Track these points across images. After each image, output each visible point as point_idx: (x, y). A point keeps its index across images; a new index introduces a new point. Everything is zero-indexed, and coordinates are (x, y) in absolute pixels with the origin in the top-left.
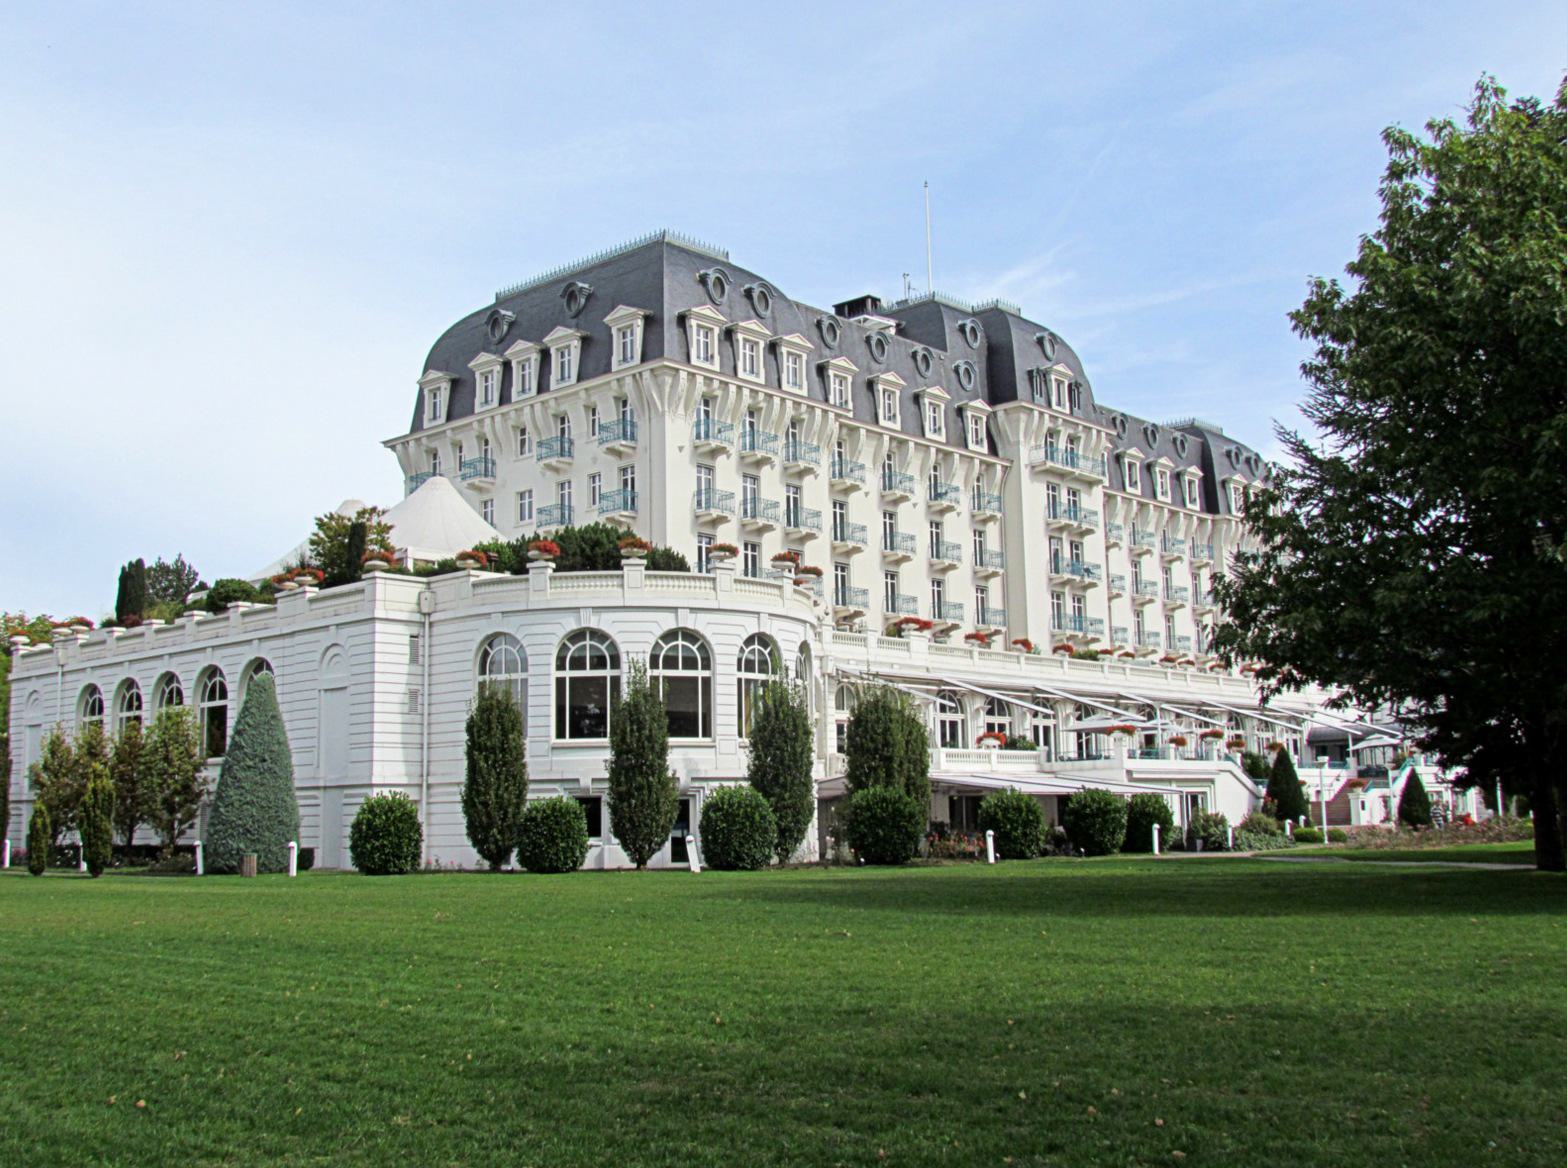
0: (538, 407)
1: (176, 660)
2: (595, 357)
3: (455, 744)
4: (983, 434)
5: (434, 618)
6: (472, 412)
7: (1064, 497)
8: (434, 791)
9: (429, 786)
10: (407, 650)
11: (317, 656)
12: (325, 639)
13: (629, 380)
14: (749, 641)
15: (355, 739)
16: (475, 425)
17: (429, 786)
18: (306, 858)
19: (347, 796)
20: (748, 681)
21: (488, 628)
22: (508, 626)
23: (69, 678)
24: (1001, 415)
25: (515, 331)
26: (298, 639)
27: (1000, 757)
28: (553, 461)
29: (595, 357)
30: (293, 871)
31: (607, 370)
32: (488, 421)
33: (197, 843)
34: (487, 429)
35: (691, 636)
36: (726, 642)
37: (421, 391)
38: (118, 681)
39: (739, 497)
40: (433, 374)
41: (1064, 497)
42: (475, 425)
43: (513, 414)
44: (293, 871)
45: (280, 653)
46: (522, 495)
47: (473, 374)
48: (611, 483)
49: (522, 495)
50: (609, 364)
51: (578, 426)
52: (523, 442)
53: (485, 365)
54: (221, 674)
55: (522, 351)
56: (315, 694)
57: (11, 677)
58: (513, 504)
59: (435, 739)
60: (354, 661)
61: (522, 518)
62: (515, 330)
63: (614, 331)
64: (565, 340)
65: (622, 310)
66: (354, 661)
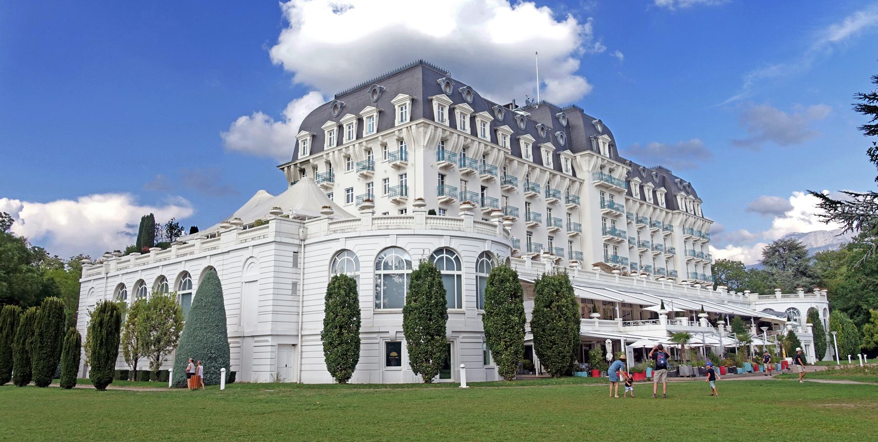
0: (357, 146)
1: (166, 268)
2: (386, 121)
3: (317, 312)
4: (570, 167)
5: (307, 242)
6: (323, 150)
7: (607, 198)
8: (305, 338)
9: (302, 336)
10: (291, 260)
11: (242, 264)
12: (247, 254)
13: (404, 130)
14: (481, 256)
15: (263, 309)
16: (325, 156)
17: (302, 336)
18: (231, 377)
19: (256, 342)
20: (481, 277)
21: (338, 246)
22: (349, 245)
23: (110, 280)
24: (578, 157)
25: (345, 111)
26: (256, 339)
27: (599, 323)
28: (365, 172)
29: (386, 121)
30: (223, 386)
31: (393, 126)
32: (331, 154)
33: (170, 370)
34: (331, 158)
35: (449, 251)
36: (468, 254)
37: (297, 141)
38: (135, 281)
39: (459, 191)
40: (303, 133)
41: (607, 198)
42: (325, 156)
43: (344, 150)
44: (223, 386)
45: (221, 263)
46: (348, 191)
47: (324, 132)
48: (394, 182)
49: (348, 191)
50: (394, 124)
51: (378, 153)
52: (349, 164)
53: (330, 125)
54: (190, 276)
55: (348, 119)
56: (239, 285)
57: (81, 280)
58: (344, 195)
59: (305, 309)
60: (263, 265)
61: (348, 202)
62: (343, 110)
63: (396, 107)
64: (370, 112)
65: (401, 96)
66: (263, 265)
